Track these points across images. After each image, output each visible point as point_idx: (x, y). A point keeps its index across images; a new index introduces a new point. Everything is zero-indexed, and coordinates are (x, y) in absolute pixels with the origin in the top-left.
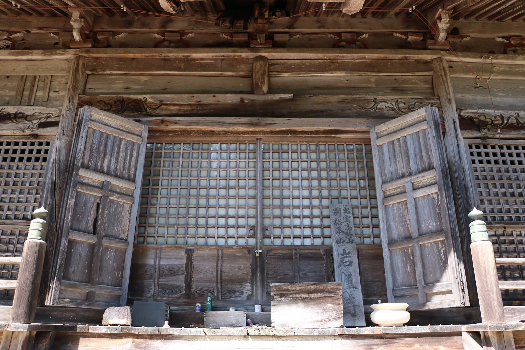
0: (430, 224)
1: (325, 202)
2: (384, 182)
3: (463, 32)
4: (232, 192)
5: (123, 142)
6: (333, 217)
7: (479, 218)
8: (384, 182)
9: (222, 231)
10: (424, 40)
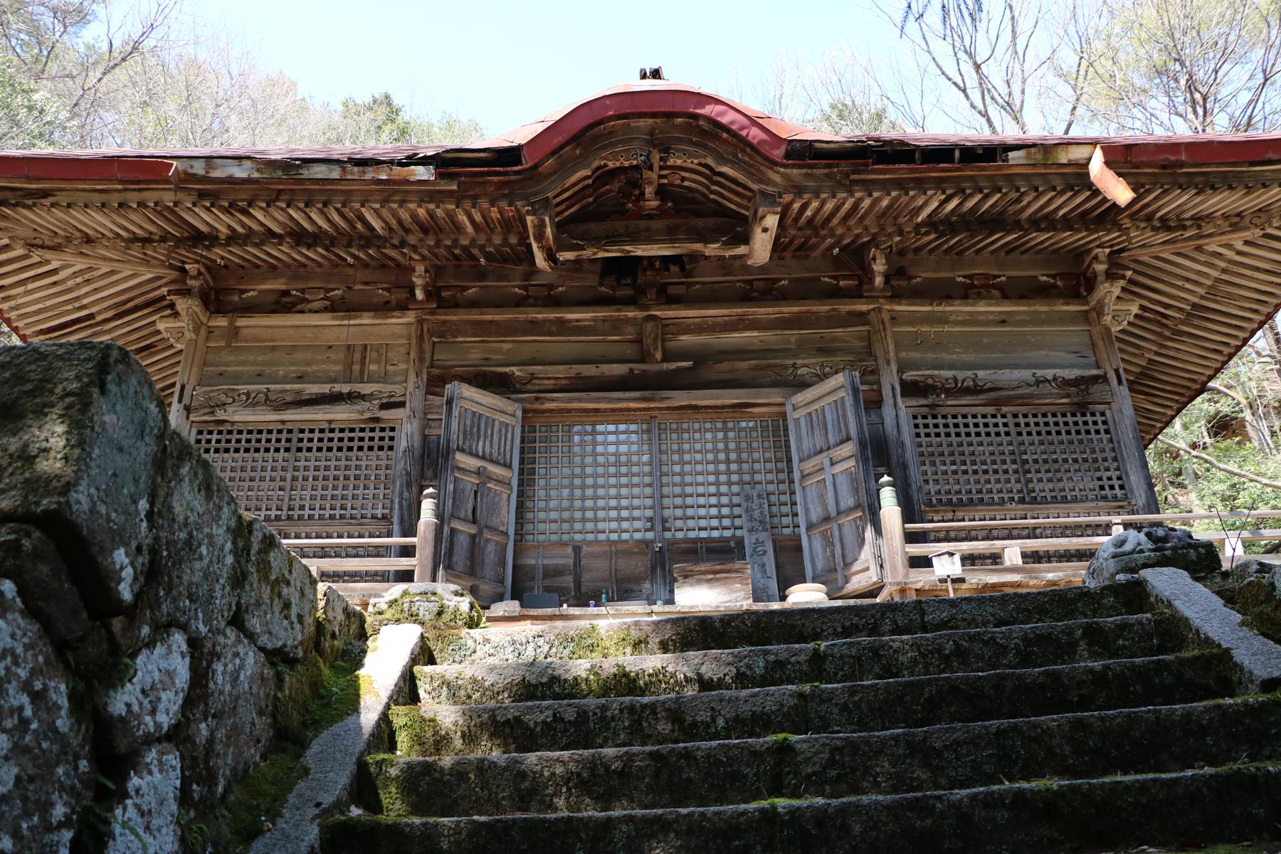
0: (848, 501)
1: (735, 489)
2: (801, 461)
3: (912, 272)
4: (624, 480)
5: (497, 423)
6: (744, 505)
7: (889, 484)
8: (801, 461)
9: (614, 525)
10: (860, 285)
